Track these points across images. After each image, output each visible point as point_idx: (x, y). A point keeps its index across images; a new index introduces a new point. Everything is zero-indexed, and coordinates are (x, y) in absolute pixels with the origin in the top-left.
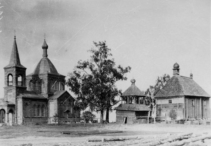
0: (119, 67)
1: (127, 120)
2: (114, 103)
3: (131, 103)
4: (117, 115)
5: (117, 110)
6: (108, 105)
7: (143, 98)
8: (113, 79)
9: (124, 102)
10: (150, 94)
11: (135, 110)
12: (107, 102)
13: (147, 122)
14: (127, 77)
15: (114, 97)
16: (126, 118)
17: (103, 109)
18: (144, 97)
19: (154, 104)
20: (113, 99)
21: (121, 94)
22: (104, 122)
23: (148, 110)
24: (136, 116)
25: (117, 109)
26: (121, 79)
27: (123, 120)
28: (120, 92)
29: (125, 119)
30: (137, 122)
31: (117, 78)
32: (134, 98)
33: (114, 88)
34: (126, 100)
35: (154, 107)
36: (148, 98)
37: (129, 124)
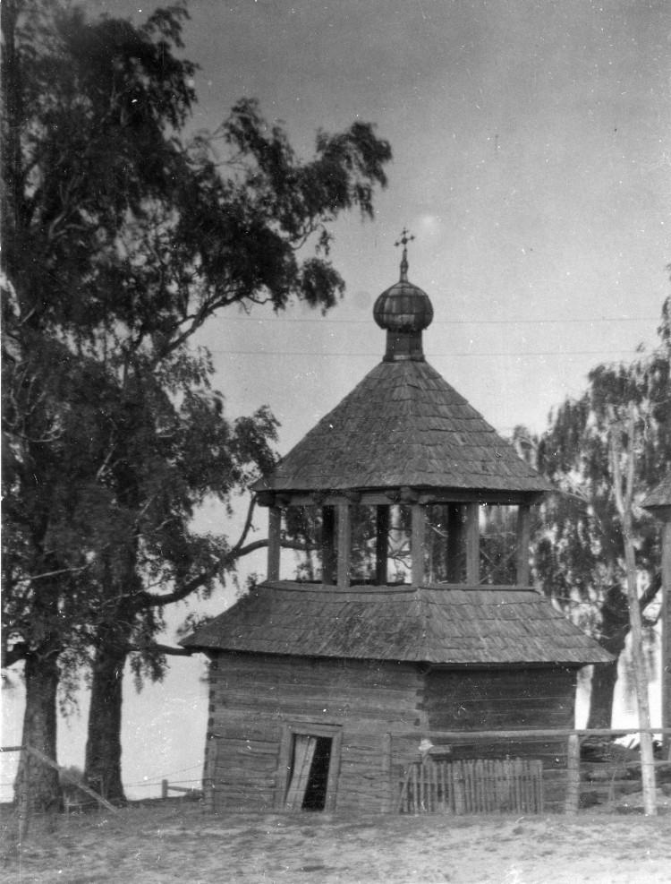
0: (246, 132)
1: (333, 767)
2: (180, 574)
3: (382, 567)
4: (231, 715)
5: (213, 653)
6: (110, 591)
7: (514, 508)
8: (173, 288)
9: (291, 563)
10: (598, 470)
11: (594, 661)
12: (104, 557)
13: (560, 793)
14: (338, 262)
15: (188, 505)
16: (324, 746)
17: (52, 645)
18: (527, 499)
19: (647, 584)
20: (177, 525)
21: (267, 465)
22: (71, 789)
23: (573, 656)
24: (434, 725)
25: (213, 641)
26: (264, 293)
27: (283, 770)
28: (252, 438)
29: (306, 753)
30: (442, 793)
31: (212, 270)
32: (419, 517)
33: (177, 399)
34: (326, 538)
35: (647, 623)
36: (571, 507)
37: (351, 821)
